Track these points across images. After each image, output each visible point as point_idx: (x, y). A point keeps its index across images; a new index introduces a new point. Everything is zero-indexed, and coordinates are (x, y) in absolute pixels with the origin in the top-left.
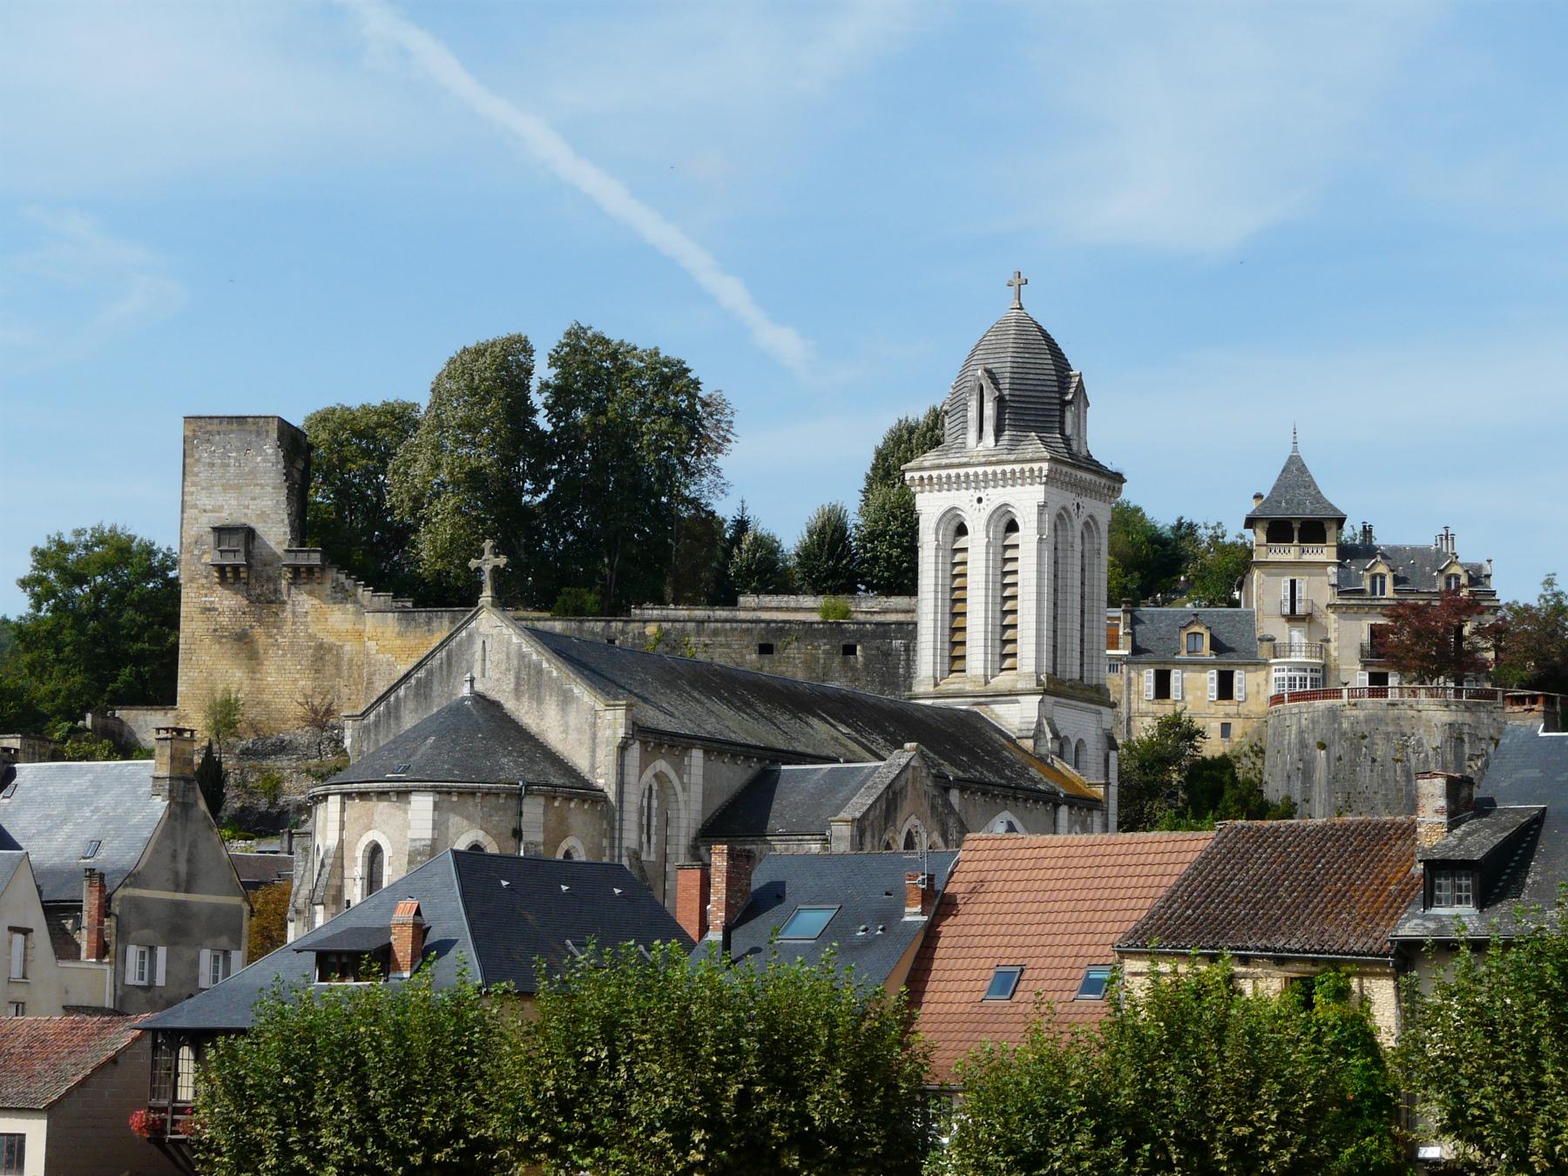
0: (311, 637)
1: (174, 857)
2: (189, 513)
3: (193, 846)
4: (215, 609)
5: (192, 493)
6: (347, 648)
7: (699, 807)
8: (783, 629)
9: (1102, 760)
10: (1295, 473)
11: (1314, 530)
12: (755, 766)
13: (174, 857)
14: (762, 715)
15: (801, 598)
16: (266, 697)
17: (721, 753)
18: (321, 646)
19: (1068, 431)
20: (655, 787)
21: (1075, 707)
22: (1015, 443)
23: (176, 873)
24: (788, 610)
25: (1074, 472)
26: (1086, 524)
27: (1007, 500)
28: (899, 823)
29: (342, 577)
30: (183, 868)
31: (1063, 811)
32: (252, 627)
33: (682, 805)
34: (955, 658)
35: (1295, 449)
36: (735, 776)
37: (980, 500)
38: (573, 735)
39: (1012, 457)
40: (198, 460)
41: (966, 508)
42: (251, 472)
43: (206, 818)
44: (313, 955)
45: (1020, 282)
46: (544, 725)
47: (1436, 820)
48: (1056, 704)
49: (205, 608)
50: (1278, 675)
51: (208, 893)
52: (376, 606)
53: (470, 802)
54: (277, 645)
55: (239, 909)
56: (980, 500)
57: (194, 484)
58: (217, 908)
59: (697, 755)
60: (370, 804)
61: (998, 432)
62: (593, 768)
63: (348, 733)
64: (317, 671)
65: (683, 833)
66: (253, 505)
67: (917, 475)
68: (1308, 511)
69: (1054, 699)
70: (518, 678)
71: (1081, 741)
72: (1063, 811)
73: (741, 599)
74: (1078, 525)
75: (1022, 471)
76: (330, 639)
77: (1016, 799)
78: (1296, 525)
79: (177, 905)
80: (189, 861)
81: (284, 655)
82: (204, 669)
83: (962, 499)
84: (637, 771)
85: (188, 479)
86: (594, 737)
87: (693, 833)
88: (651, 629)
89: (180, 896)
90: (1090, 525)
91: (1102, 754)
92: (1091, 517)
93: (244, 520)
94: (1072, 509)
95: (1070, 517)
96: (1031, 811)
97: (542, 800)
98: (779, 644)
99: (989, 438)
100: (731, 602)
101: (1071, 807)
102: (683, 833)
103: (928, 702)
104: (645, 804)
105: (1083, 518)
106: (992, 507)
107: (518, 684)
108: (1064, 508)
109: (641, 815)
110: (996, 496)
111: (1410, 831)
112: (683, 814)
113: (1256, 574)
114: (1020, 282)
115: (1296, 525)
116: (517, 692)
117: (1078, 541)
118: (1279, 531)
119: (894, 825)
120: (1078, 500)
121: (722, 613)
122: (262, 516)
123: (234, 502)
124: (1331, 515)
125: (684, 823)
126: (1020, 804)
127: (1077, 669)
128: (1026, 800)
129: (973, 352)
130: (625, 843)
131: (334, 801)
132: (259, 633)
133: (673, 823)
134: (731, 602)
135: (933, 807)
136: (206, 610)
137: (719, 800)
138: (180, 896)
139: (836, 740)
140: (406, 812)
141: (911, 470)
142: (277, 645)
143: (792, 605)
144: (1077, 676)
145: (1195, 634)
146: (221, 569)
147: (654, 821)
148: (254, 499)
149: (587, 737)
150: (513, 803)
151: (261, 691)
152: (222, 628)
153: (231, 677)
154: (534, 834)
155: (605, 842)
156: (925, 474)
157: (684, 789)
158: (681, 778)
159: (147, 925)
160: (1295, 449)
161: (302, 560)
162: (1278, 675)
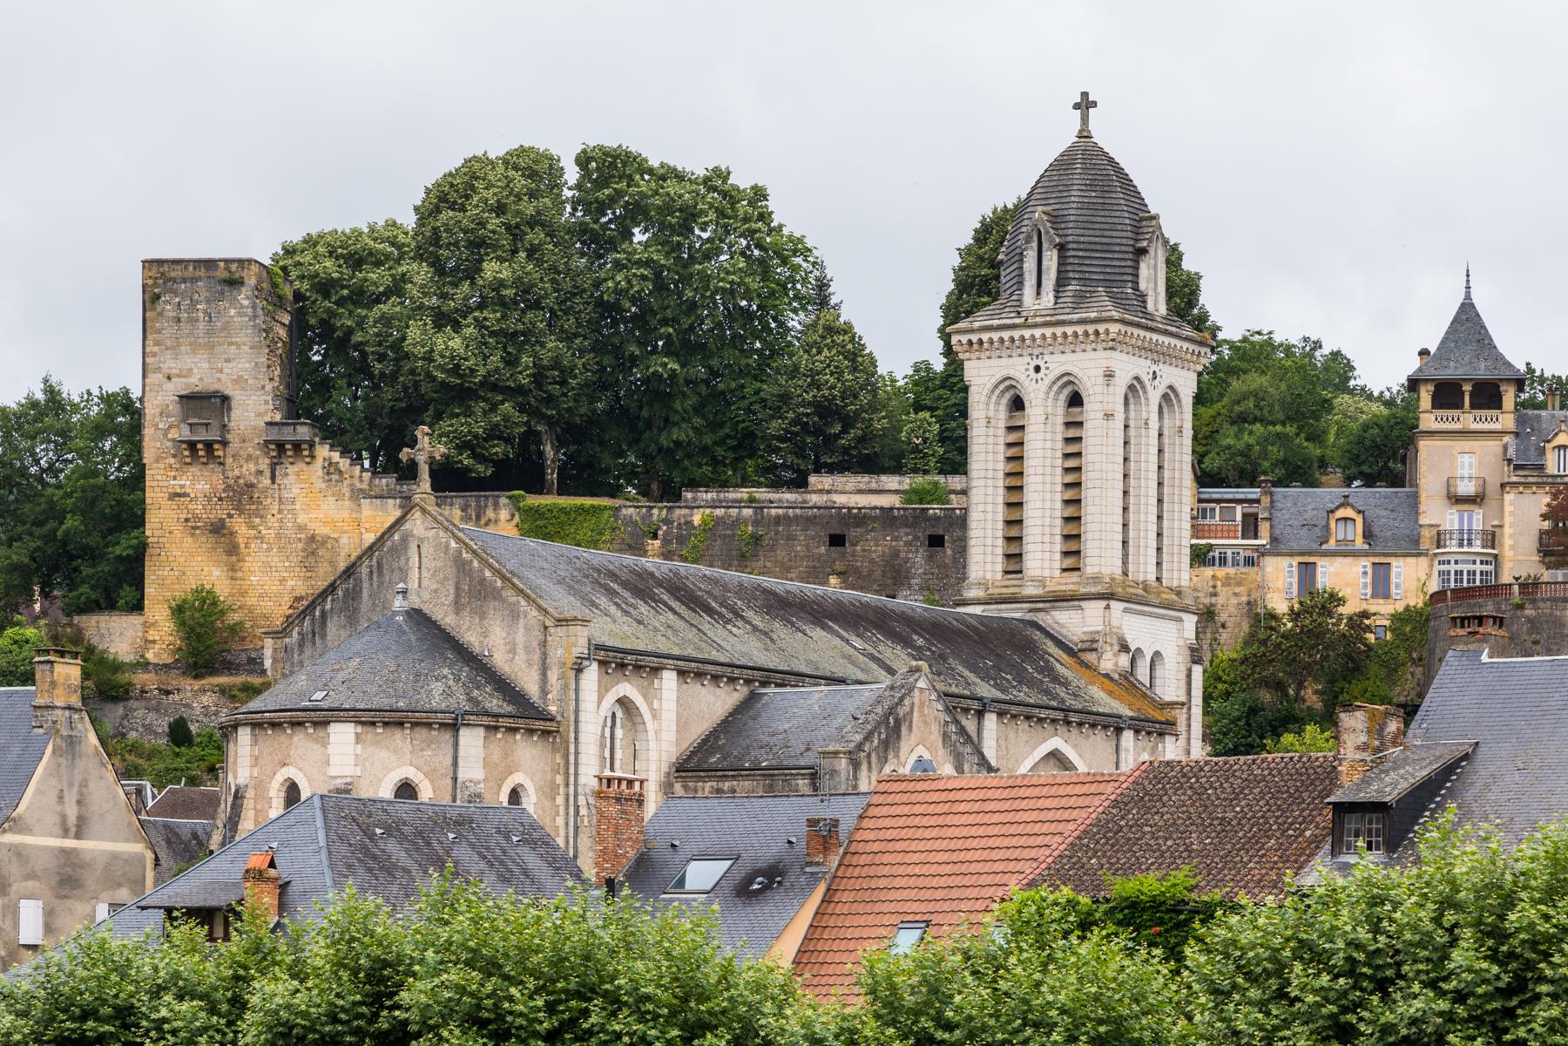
0: (301, 528)
1: (61, 798)
2: (153, 378)
3: (84, 784)
4: (185, 495)
5: (155, 355)
6: (344, 540)
7: (672, 736)
8: (859, 518)
9: (1183, 676)
10: (1467, 325)
11: (1487, 395)
12: (742, 691)
13: (61, 798)
14: (755, 628)
15: (883, 478)
16: (251, 600)
17: (699, 675)
18: (312, 538)
19: (1143, 286)
20: (619, 714)
21: (1150, 615)
22: (1081, 300)
23: (64, 817)
24: (871, 491)
25: (1148, 335)
26: (1165, 397)
27: (1068, 368)
28: (903, 752)
29: (336, 456)
30: (72, 812)
31: (1128, 735)
32: (230, 516)
33: (651, 735)
34: (1014, 560)
35: (1468, 296)
36: (717, 702)
37: (1037, 369)
38: (521, 658)
39: (1075, 317)
40: (161, 314)
41: (1022, 378)
42: (223, 329)
43: (98, 753)
44: (689, 886)
45: (1085, 104)
46: (490, 641)
47: (1358, 756)
48: (1125, 610)
49: (173, 494)
50: (1443, 567)
51: (101, 839)
52: (378, 491)
53: (370, 729)
54: (260, 537)
55: (142, 859)
56: (1037, 369)
57: (157, 343)
58: (115, 856)
59: (669, 678)
60: (283, 738)
61: (1061, 283)
62: (544, 692)
63: (268, 653)
64: (309, 569)
65: (653, 767)
66: (227, 368)
67: (964, 339)
68: (1483, 371)
69: (1122, 605)
70: (457, 588)
71: (1157, 654)
72: (1128, 735)
73: (812, 479)
74: (1155, 397)
75: (1054, 336)
76: (321, 530)
77: (1068, 723)
78: (1467, 388)
79: (64, 852)
80: (79, 802)
81: (269, 550)
82: (178, 564)
83: (1017, 367)
84: (595, 697)
85: (150, 337)
86: (544, 656)
87: (665, 768)
88: (697, 519)
89: (70, 843)
90: (1169, 398)
91: (1183, 668)
92: (1171, 387)
93: (216, 387)
94: (1146, 378)
95: (1143, 387)
96: (1087, 737)
97: (481, 732)
98: (853, 533)
99: (1048, 298)
100: (800, 483)
101: (1137, 732)
102: (653, 767)
103: (977, 610)
104: (608, 734)
105: (1161, 389)
106: (1052, 377)
107: (458, 596)
108: (1137, 378)
109: (602, 746)
110: (1057, 364)
111: (1332, 774)
112: (652, 745)
113: (1424, 445)
114: (1085, 104)
115: (1467, 388)
116: (458, 607)
117: (1154, 416)
118: (1447, 395)
119: (897, 756)
120: (1154, 368)
121: (789, 496)
122: (239, 381)
123: (206, 365)
124: (1508, 374)
125: (653, 756)
126: (1075, 731)
127: (1152, 568)
128: (1080, 724)
129: (1034, 188)
130: (582, 780)
131: (244, 735)
132: (239, 526)
133: (641, 755)
134: (800, 483)
135: (946, 736)
136: (175, 496)
137: (699, 729)
138: (70, 843)
139: (849, 658)
140: (325, 744)
141: (959, 332)
142: (260, 537)
143: (874, 486)
144: (1152, 577)
145: (1346, 519)
146: (192, 445)
147: (619, 754)
148: (228, 361)
149: (536, 657)
150: (447, 736)
151: (243, 593)
152: (196, 517)
153: (210, 574)
154: (472, 770)
155: (559, 779)
156: (974, 338)
157: (654, 717)
158: (650, 704)
159: (31, 876)
160: (1468, 296)
161: (288, 434)
162: (1443, 567)
